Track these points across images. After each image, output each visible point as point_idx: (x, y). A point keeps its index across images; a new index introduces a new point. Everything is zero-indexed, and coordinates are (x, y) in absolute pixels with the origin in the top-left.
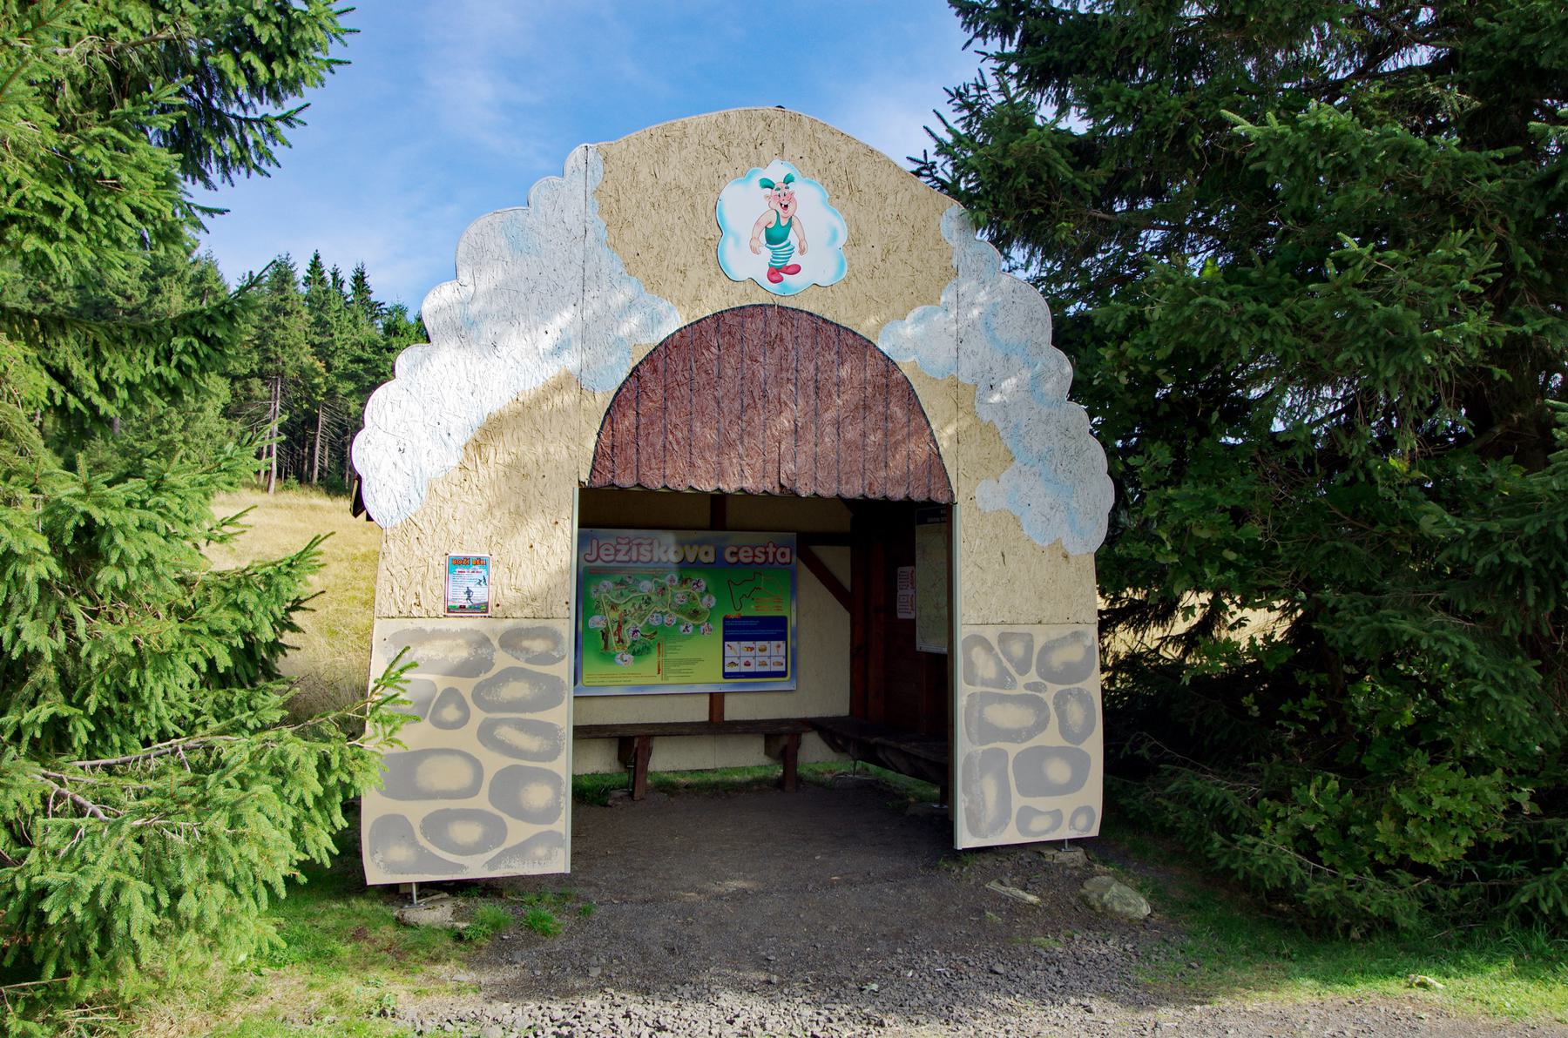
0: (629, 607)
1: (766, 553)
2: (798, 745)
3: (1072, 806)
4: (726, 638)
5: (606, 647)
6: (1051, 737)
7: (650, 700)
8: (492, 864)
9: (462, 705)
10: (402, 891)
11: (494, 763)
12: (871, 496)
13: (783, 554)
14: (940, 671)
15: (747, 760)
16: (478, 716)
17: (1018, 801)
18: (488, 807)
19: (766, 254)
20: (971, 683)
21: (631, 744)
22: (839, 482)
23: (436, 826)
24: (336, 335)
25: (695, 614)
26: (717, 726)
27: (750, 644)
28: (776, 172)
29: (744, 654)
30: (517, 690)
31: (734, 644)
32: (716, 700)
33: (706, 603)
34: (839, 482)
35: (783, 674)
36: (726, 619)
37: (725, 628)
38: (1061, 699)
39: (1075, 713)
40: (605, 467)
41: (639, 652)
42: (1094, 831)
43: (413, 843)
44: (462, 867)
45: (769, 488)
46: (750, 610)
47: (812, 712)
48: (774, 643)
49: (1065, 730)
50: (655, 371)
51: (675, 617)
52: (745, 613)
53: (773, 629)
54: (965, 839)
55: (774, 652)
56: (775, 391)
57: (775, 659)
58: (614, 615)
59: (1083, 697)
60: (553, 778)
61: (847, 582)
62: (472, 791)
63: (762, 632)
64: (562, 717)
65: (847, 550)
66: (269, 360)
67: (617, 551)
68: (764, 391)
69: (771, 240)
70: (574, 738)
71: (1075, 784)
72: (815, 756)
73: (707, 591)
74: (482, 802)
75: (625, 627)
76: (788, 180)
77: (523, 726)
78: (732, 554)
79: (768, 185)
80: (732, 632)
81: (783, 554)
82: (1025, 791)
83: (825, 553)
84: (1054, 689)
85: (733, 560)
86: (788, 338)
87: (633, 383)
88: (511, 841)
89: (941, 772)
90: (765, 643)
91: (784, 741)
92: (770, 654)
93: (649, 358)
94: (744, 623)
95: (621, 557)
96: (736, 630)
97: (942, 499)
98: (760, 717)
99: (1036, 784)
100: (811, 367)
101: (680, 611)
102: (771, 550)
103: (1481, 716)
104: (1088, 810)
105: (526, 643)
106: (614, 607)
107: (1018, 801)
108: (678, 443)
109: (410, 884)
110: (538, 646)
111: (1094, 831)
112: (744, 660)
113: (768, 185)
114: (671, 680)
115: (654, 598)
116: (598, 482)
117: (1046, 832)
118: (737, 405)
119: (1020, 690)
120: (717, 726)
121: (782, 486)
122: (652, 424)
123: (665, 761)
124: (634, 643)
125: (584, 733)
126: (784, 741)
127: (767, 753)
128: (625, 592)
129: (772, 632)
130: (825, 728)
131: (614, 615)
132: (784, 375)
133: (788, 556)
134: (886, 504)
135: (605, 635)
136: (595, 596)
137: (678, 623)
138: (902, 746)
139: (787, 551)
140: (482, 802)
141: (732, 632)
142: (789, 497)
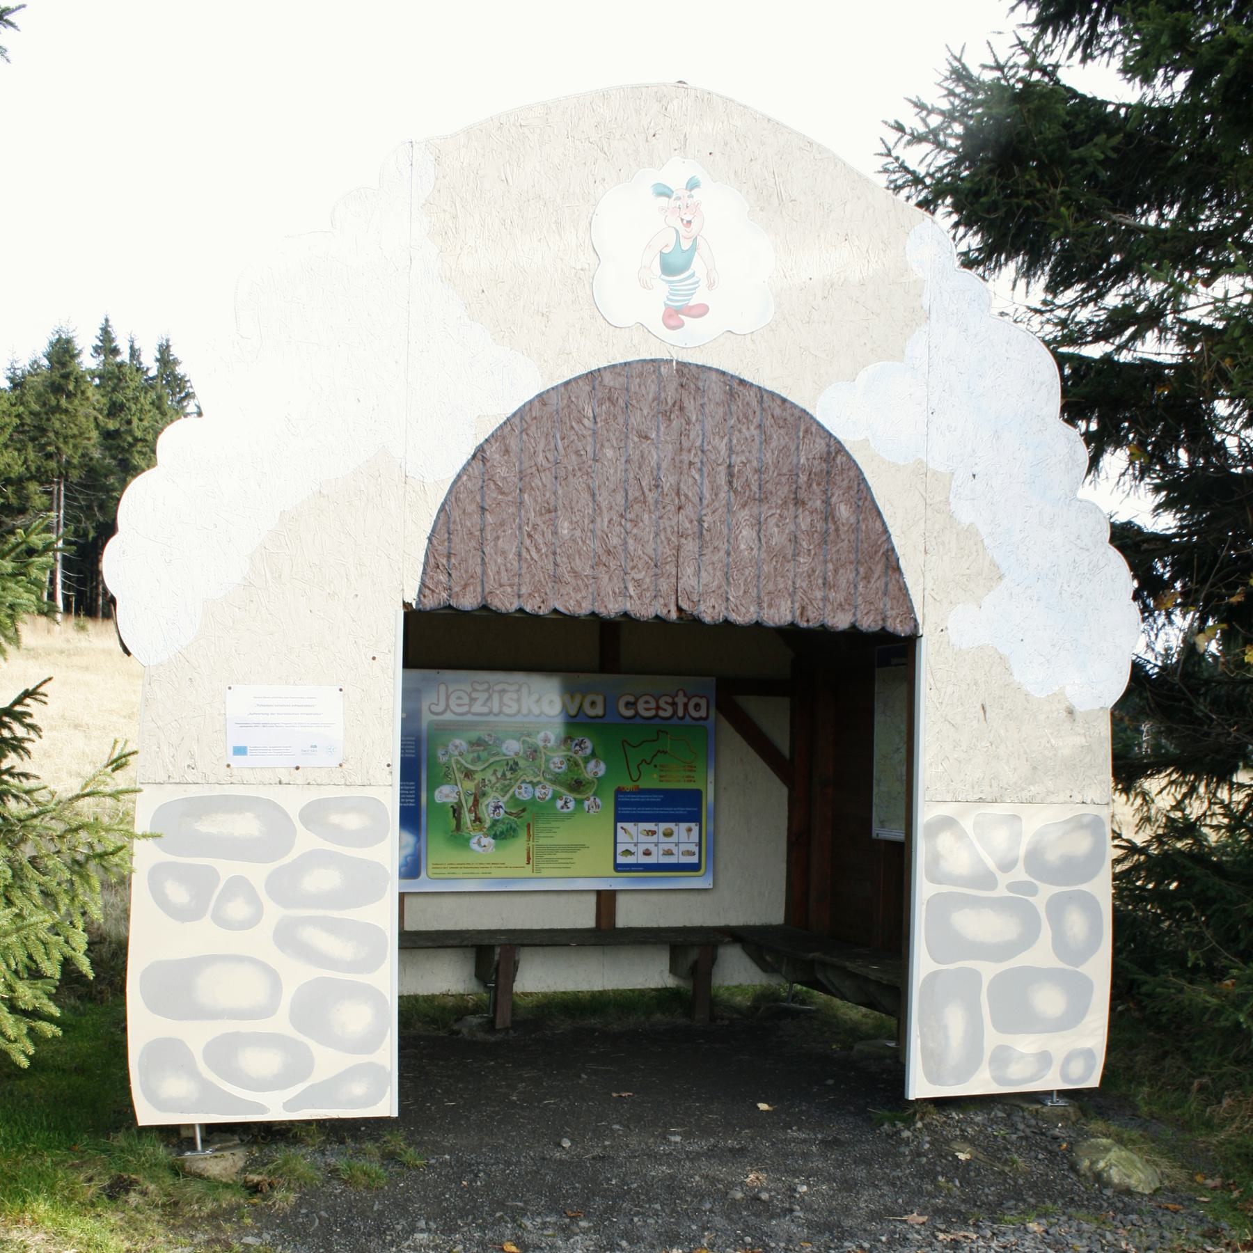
0: (489, 775)
1: (674, 704)
2: (713, 960)
3: (1064, 1044)
4: (619, 818)
5: (458, 827)
6: (1041, 954)
7: (517, 899)
8: (288, 1106)
9: (253, 899)
10: (184, 1133)
11: (297, 975)
12: (803, 624)
13: (697, 707)
14: (896, 861)
15: (650, 974)
16: (273, 913)
17: (992, 1038)
18: (290, 1031)
19: (660, 292)
20: (934, 879)
21: (492, 954)
22: (760, 605)
23: (223, 1053)
24: (135, 421)
25: (577, 786)
26: (605, 935)
27: (651, 826)
28: (675, 173)
29: (642, 840)
30: (322, 880)
31: (629, 826)
32: (606, 901)
33: (595, 769)
34: (760, 605)
35: (695, 868)
36: (619, 792)
37: (618, 804)
38: (1057, 907)
39: (1076, 924)
40: (439, 582)
41: (502, 834)
42: (1094, 1081)
43: (194, 1074)
44: (263, 1109)
45: (663, 612)
46: (651, 781)
47: (735, 919)
48: (684, 826)
49: (1061, 945)
50: (507, 451)
51: (550, 790)
52: (644, 784)
53: (682, 806)
54: (919, 1086)
55: (684, 835)
56: (672, 480)
57: (683, 847)
58: (470, 786)
59: (1088, 902)
60: (372, 995)
61: (783, 743)
62: (266, 1011)
63: (670, 810)
64: (384, 919)
65: (785, 702)
66: (49, 456)
67: (473, 700)
68: (657, 479)
69: (670, 268)
70: (401, 948)
71: (1073, 1017)
72: (737, 975)
73: (593, 754)
74: (280, 1023)
75: (484, 802)
76: (692, 185)
77: (333, 927)
78: (628, 704)
79: (663, 192)
80: (626, 810)
81: (697, 707)
82: (1003, 1025)
83: (754, 706)
84: (1046, 891)
85: (630, 713)
86: (690, 405)
87: (478, 465)
88: (318, 1077)
89: (891, 996)
90: (671, 825)
91: (693, 955)
92: (680, 840)
93: (498, 436)
94: (644, 798)
95: (477, 708)
96: (631, 807)
97: (901, 629)
98: (663, 923)
99: (1017, 1017)
100: (723, 447)
101: (556, 780)
102: (681, 700)
103: (1231, 829)
104: (1088, 1054)
105: (335, 819)
106: (468, 774)
107: (992, 1038)
108: (538, 550)
109: (192, 1126)
110: (352, 822)
111: (1094, 1081)
112: (642, 848)
113: (663, 192)
114: (545, 873)
115: (522, 763)
116: (430, 603)
117: (1031, 1079)
118: (620, 498)
119: (1001, 892)
120: (605, 935)
121: (680, 609)
122: (502, 524)
123: (537, 978)
124: (495, 822)
125: (413, 943)
126: (693, 955)
127: (673, 970)
128: (484, 755)
129: (681, 811)
130: (750, 939)
131: (470, 786)
132: (685, 457)
133: (702, 709)
134: (823, 635)
135: (456, 811)
136: (443, 759)
137: (556, 796)
138: (850, 965)
139: (703, 702)
140: (280, 1023)
141: (626, 810)
142: (690, 623)
